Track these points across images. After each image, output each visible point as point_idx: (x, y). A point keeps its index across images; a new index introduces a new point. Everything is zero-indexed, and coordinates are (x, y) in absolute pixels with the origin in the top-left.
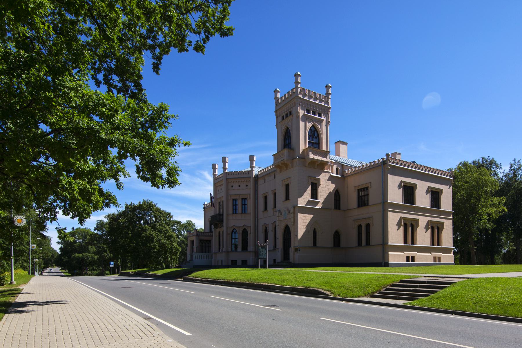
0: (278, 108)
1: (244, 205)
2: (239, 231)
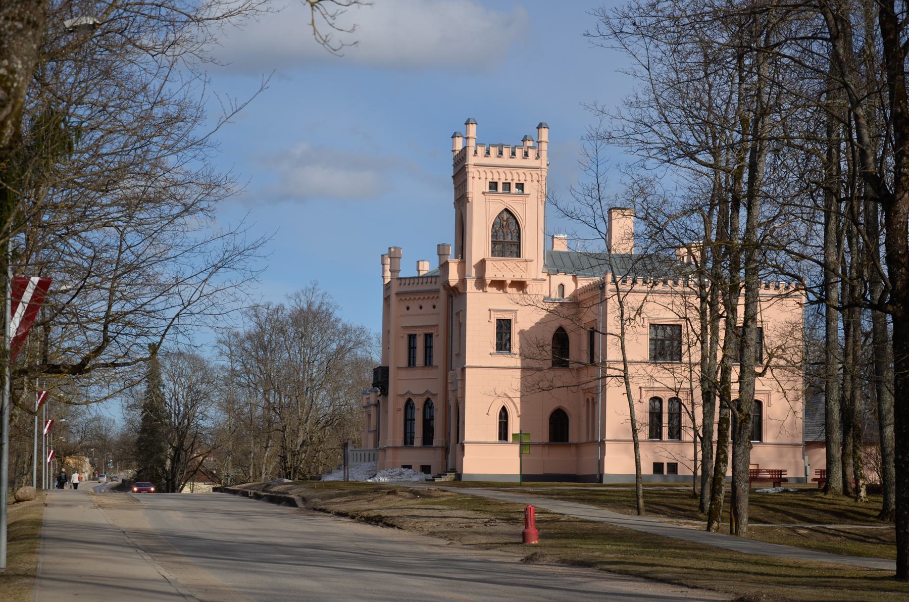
1: (428, 348)
2: (419, 404)
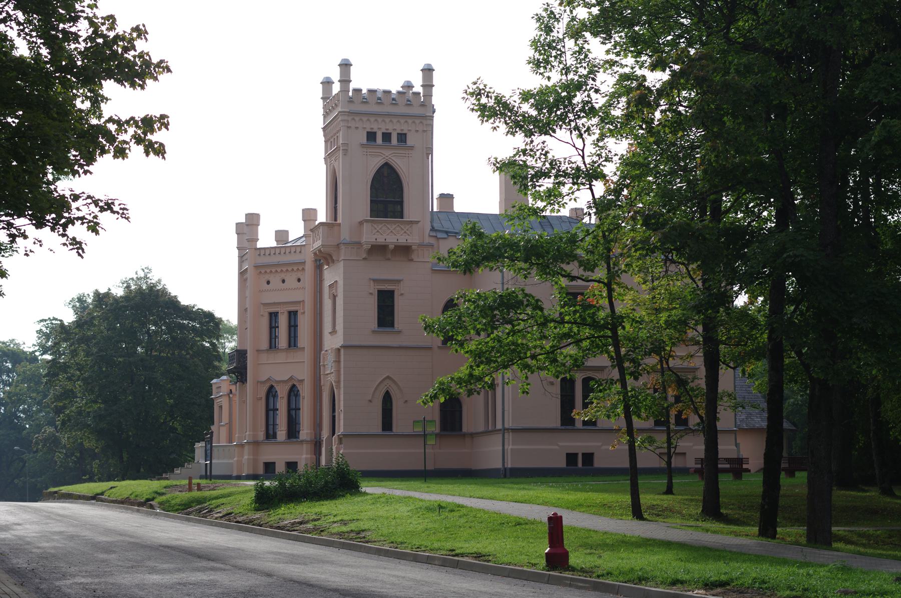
1: (293, 327)
2: (282, 392)
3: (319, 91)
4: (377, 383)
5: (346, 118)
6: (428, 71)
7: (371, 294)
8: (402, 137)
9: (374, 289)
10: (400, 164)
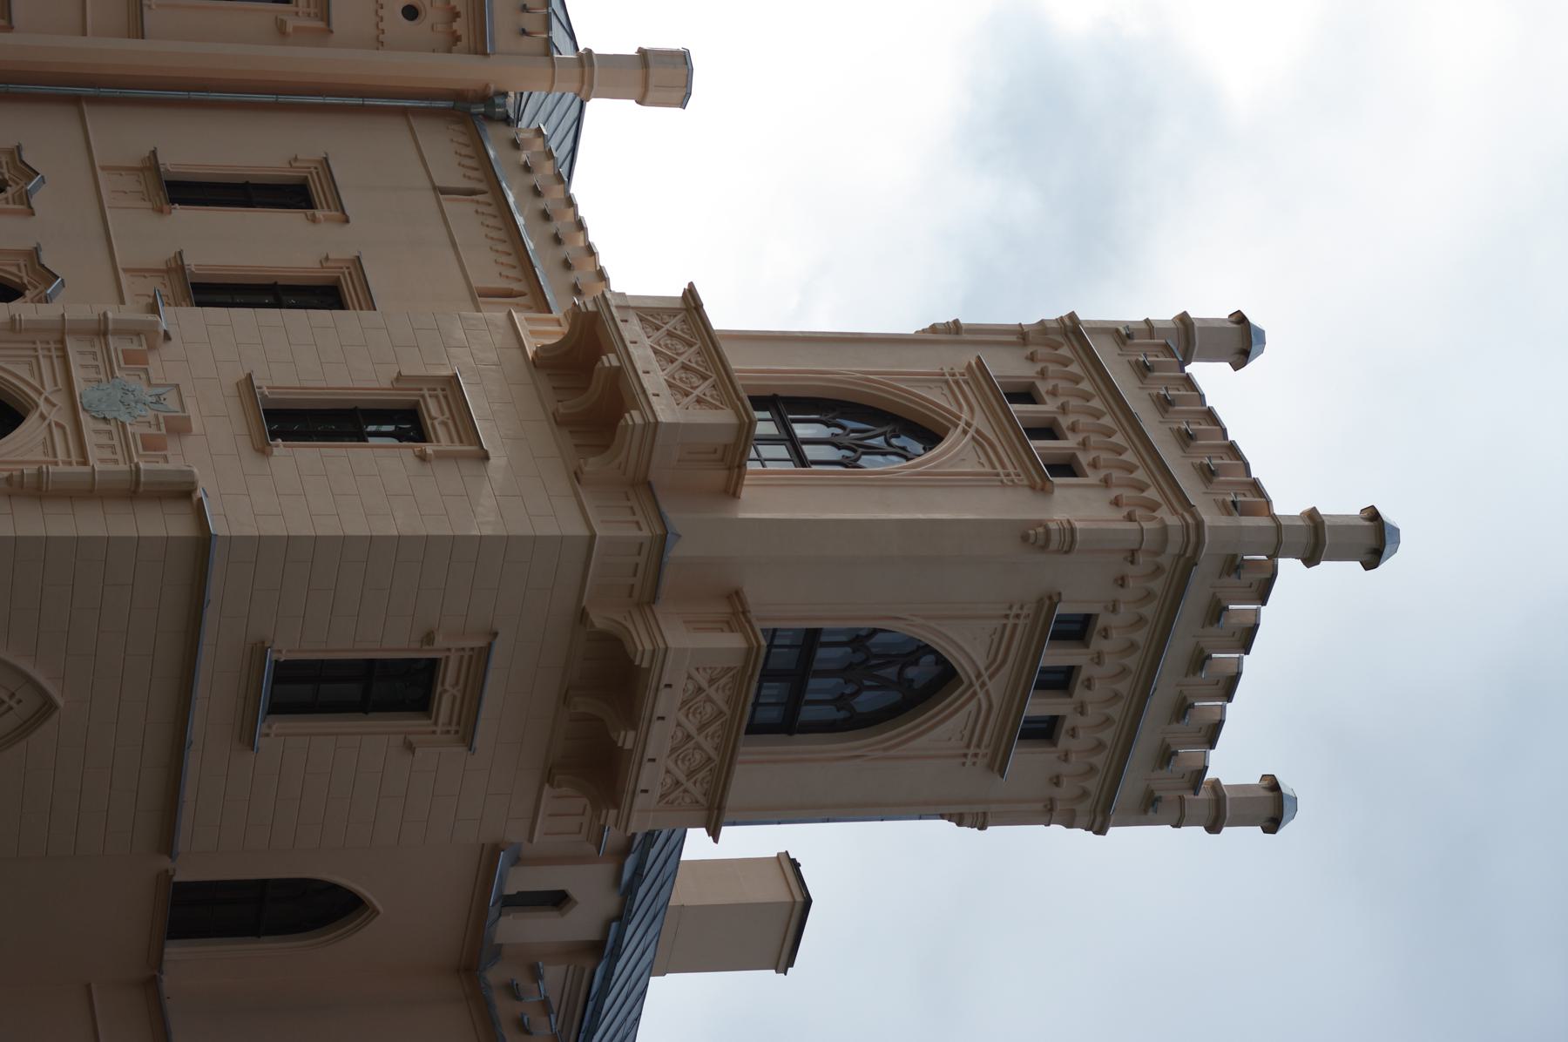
0: (1105, 352)
3: (1211, 307)
4: (26, 665)
5: (1173, 548)
6: (1270, 807)
7: (429, 638)
8: (1044, 731)
9: (449, 646)
10: (945, 730)
